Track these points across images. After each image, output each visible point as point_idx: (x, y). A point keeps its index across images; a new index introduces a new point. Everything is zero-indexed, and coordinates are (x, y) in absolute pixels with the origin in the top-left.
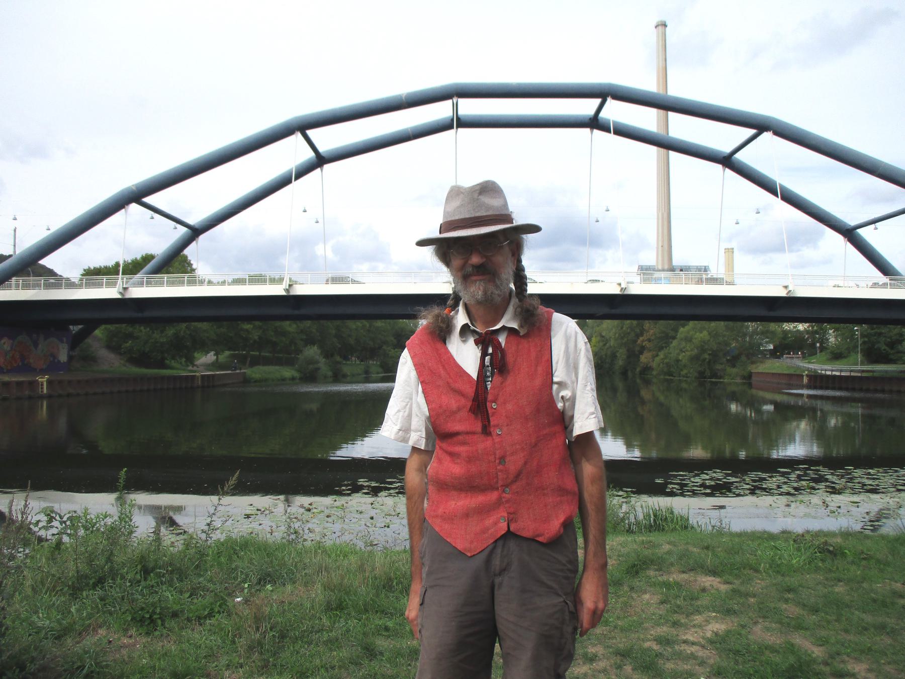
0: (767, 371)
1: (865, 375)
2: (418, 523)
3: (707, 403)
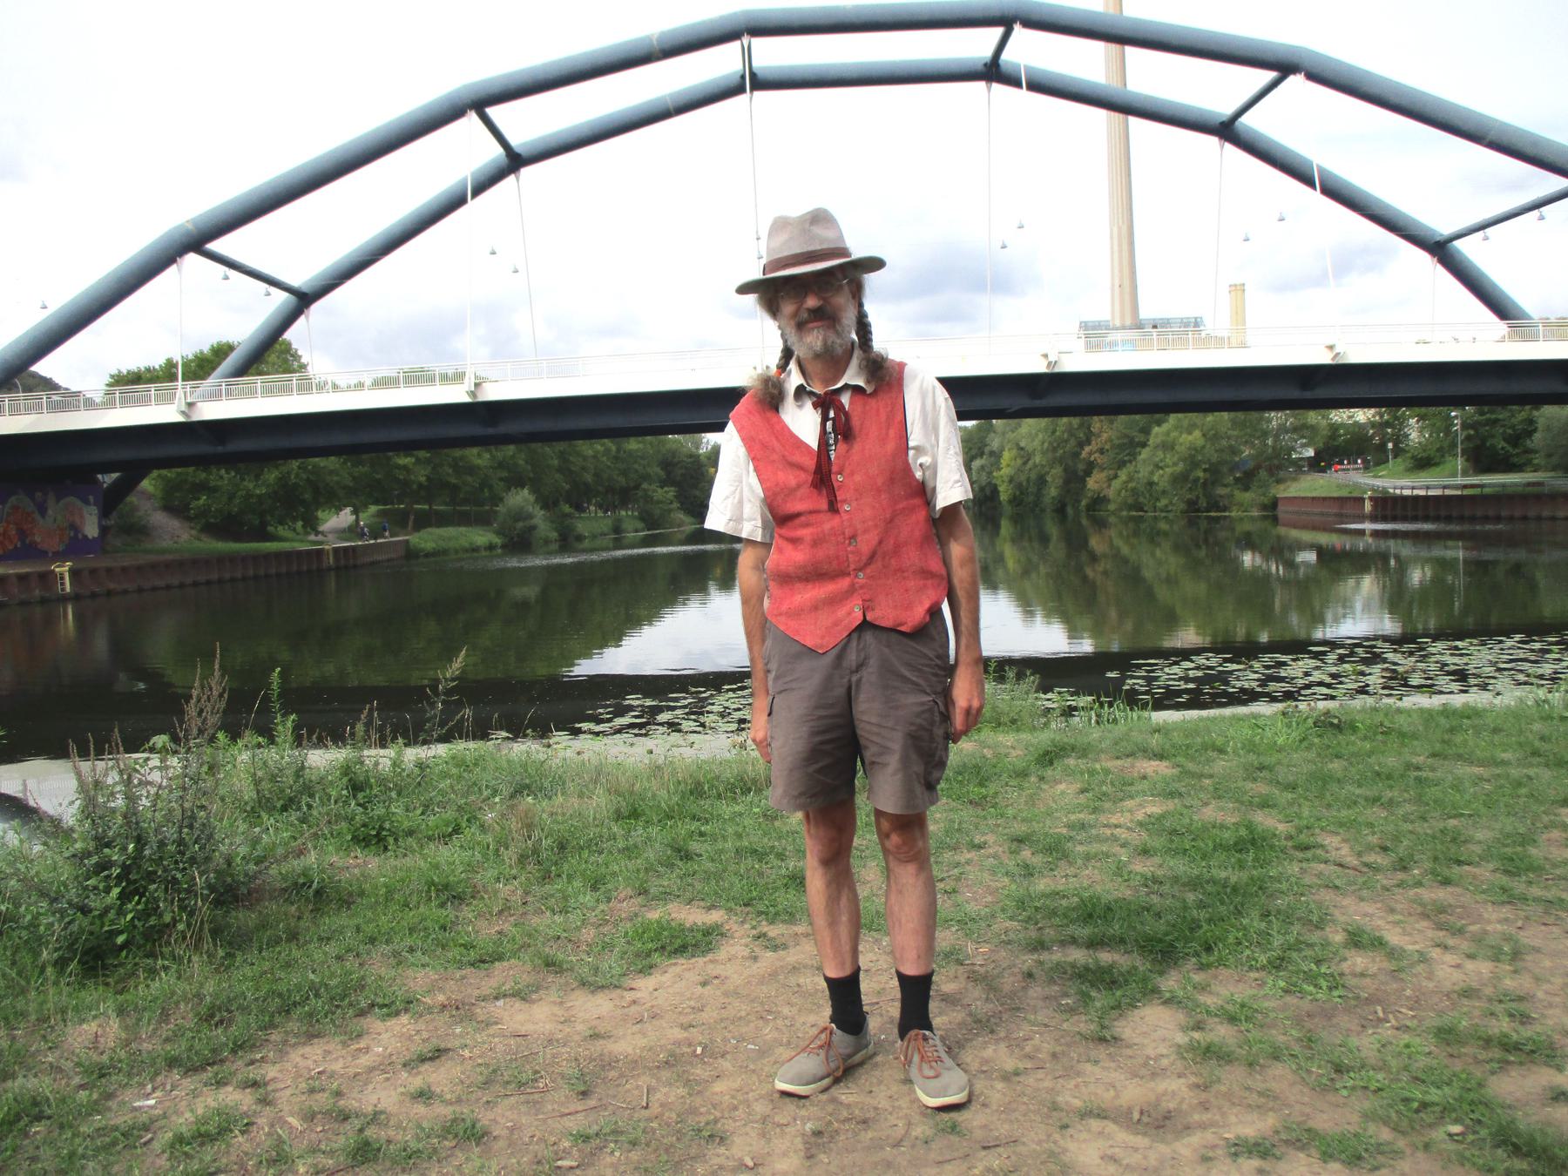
0: (1303, 494)
1: (1466, 492)
2: (757, 627)
3: (1203, 553)
